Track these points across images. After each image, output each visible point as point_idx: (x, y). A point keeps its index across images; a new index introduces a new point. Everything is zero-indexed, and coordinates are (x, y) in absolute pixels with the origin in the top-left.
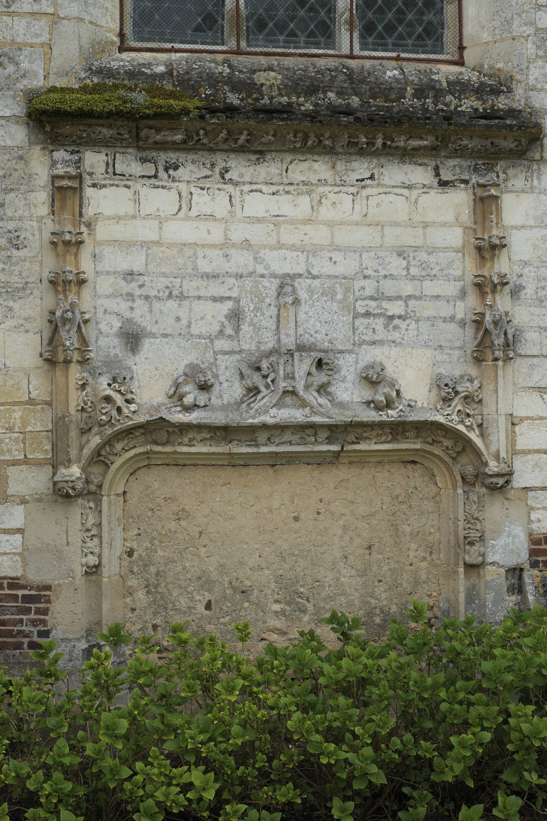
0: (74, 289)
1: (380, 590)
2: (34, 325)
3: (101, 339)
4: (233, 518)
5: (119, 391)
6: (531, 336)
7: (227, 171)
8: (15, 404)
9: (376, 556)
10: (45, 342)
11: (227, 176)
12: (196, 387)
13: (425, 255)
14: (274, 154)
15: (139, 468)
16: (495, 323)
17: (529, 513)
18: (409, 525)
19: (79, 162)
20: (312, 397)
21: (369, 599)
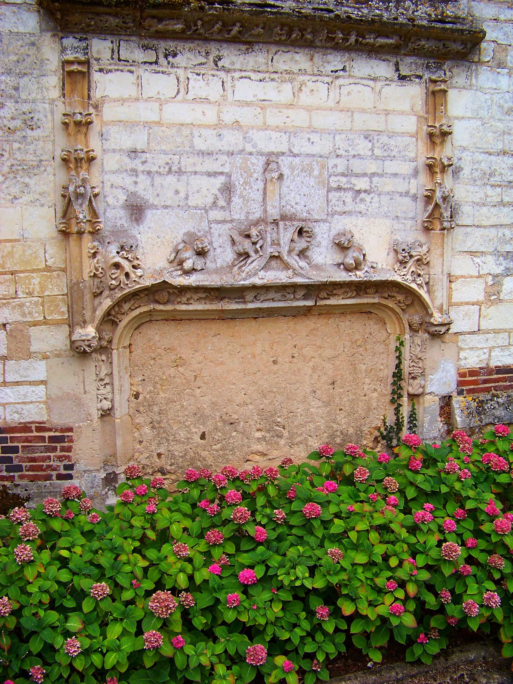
0: (85, 166)
1: (341, 418)
2: (49, 199)
3: (108, 210)
4: (222, 363)
5: (127, 258)
6: (466, 209)
7: (220, 59)
8: (33, 271)
9: (338, 390)
10: (59, 214)
11: (220, 64)
12: (194, 253)
13: (387, 138)
14: (261, 45)
15: (143, 323)
16: (445, 199)
17: (459, 353)
18: (364, 364)
19: (87, 48)
20: (293, 261)
21: (332, 424)
